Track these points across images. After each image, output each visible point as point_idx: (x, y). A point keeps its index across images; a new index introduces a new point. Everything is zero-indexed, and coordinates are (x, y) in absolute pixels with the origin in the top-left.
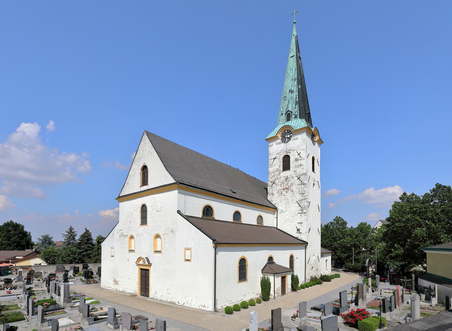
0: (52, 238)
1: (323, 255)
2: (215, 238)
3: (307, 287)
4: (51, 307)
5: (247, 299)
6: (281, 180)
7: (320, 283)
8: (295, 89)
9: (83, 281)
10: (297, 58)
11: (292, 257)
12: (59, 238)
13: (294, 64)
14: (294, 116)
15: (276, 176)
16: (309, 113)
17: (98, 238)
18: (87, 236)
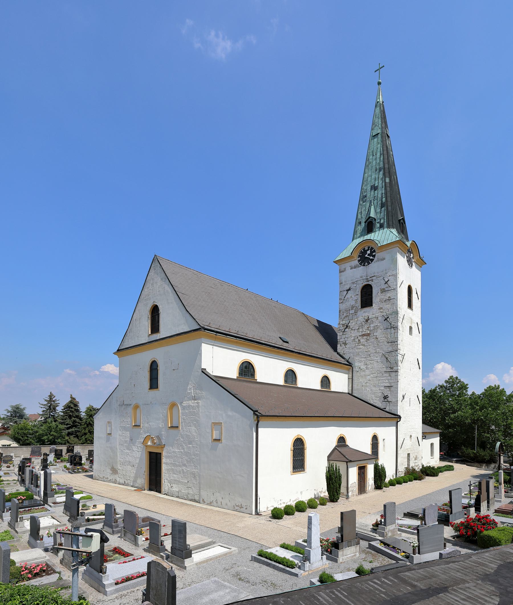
0: (24, 409)
1: (425, 436)
2: (255, 408)
3: (399, 483)
4: (26, 503)
5: (305, 498)
6: (359, 322)
7: (419, 478)
8: (379, 183)
9: (68, 469)
10: (382, 137)
11: (375, 438)
12: (34, 409)
13: (379, 145)
14: (378, 225)
15: (351, 316)
16: (403, 219)
17: (88, 408)
18: (72, 407)
